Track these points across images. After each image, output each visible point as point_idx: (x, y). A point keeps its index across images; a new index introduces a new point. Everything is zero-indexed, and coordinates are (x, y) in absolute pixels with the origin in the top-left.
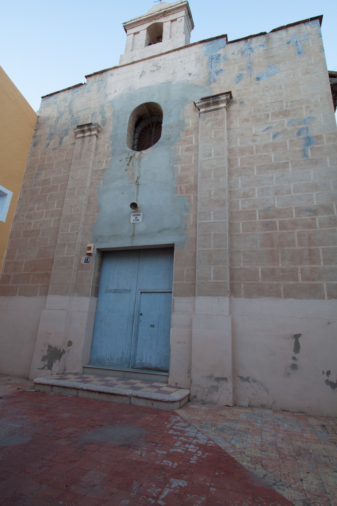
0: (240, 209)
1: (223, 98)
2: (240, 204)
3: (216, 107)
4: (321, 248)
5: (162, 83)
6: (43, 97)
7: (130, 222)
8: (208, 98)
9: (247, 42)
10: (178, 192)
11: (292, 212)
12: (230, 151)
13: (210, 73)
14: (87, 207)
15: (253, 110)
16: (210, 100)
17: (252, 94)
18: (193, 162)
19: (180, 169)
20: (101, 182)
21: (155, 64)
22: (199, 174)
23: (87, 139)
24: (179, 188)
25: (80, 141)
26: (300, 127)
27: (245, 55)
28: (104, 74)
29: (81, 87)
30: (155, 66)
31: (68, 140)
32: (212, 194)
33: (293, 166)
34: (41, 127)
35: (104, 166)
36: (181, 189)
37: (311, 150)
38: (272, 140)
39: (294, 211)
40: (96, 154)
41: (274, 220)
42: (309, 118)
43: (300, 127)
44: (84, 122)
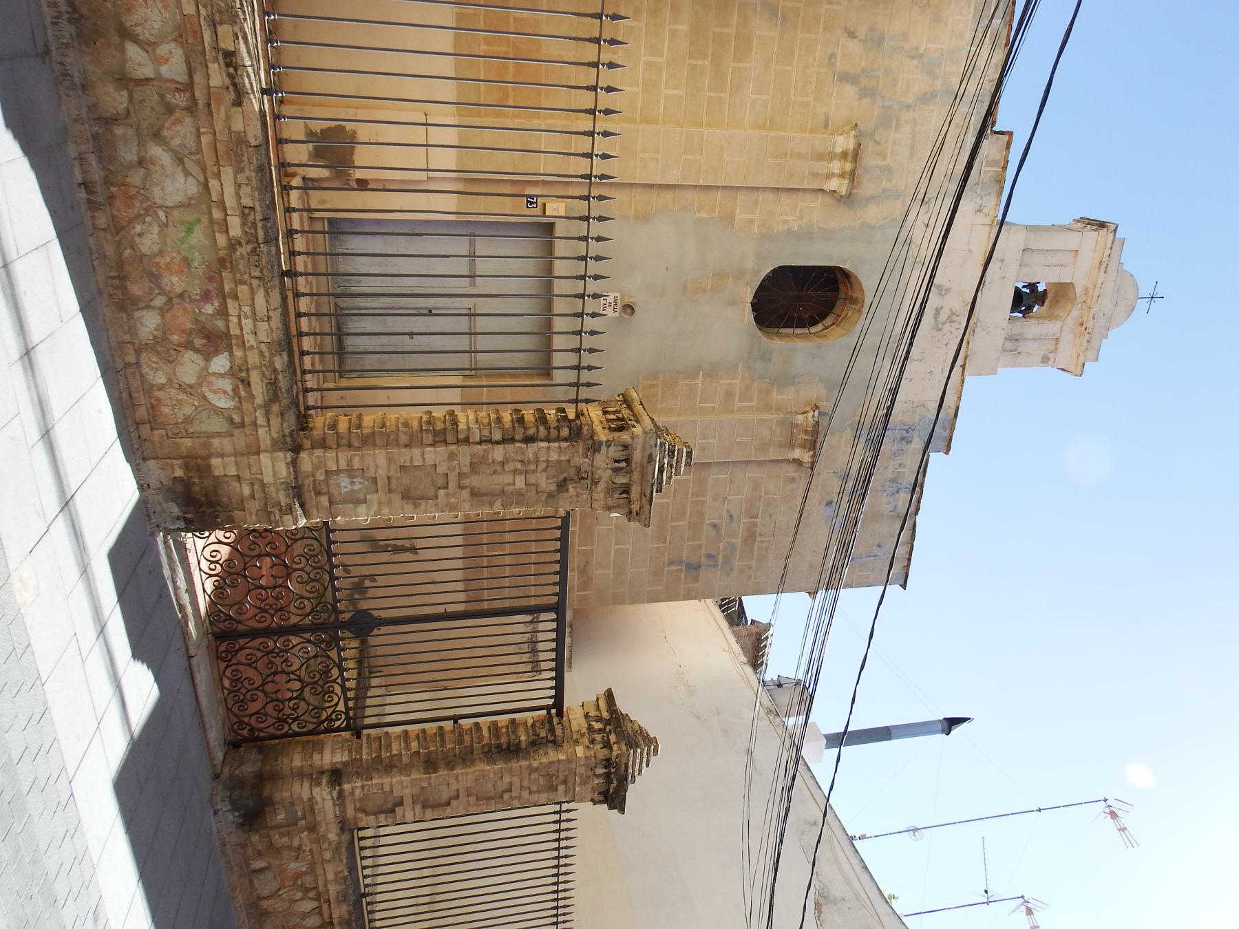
3: (476, 528)
4: (726, 95)
20: (705, 215)
33: (657, 548)
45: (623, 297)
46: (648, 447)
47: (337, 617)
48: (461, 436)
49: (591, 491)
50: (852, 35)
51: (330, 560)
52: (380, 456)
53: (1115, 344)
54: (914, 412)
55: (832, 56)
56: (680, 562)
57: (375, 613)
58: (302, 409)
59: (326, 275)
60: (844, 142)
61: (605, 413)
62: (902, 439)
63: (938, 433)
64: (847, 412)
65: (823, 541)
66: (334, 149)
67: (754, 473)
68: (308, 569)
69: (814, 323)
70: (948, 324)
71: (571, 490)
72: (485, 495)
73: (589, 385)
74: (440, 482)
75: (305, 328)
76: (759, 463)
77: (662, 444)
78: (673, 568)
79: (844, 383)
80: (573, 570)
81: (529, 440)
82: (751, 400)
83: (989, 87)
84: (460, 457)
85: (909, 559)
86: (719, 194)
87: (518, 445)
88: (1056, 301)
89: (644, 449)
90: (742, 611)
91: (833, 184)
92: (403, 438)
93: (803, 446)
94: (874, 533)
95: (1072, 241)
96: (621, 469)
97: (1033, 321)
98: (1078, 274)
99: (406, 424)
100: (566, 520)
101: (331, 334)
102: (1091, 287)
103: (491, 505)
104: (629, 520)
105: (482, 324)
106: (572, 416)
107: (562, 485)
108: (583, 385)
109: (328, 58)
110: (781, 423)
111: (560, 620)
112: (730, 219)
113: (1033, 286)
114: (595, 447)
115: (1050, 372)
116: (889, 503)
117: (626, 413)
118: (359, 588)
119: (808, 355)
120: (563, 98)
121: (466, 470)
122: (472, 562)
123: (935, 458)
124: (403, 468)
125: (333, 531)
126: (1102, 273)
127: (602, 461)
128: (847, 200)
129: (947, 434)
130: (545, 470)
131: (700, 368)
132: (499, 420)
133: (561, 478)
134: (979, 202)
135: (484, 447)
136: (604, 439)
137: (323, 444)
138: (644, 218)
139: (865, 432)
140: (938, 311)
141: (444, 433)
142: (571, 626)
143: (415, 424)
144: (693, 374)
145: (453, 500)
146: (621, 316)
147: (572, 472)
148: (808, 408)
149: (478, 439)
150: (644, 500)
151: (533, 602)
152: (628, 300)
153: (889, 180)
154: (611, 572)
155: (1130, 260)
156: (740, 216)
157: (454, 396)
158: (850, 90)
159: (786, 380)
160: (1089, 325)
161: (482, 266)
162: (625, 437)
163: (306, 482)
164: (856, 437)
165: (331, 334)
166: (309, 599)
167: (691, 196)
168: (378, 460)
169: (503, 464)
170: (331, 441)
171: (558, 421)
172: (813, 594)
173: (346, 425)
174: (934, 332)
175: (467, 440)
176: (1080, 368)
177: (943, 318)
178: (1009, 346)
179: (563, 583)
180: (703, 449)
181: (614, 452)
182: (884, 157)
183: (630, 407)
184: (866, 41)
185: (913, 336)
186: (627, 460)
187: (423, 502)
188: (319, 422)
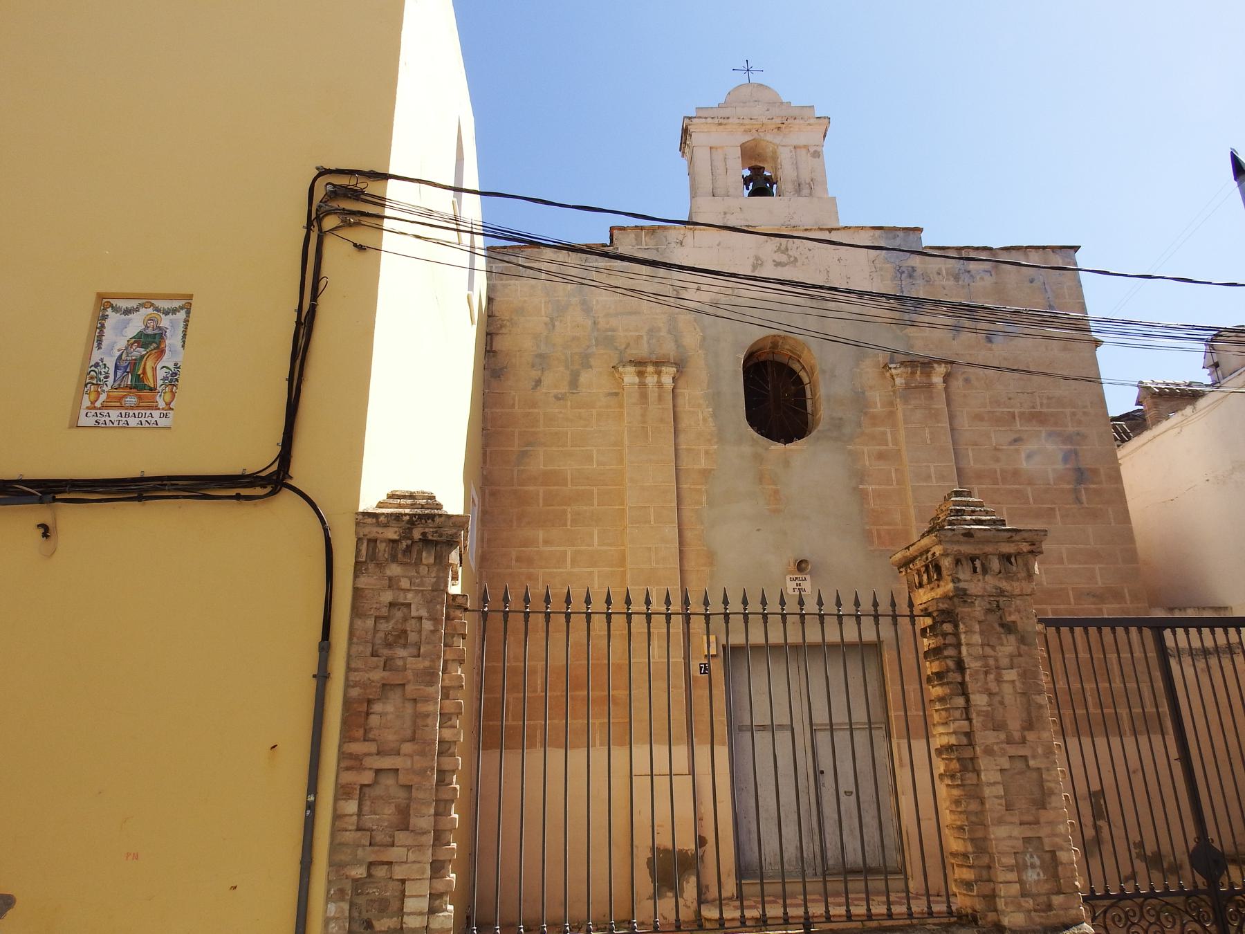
3: (1068, 722)
4: (595, 489)
20: (704, 498)
39: (1071, 593)
45: (790, 573)
46: (955, 538)
47: (1203, 892)
48: (964, 741)
49: (1012, 596)
50: (538, 382)
51: (1129, 897)
52: (998, 832)
53: (793, 94)
54: (881, 269)
55: (557, 398)
56: (1076, 491)
57: (1192, 844)
58: (953, 920)
59: (784, 883)
60: (630, 376)
61: (921, 585)
62: (910, 276)
63: (900, 243)
64: (888, 338)
65: (1029, 342)
66: (670, 869)
67: (963, 422)
68: (1144, 924)
69: (799, 381)
70: (790, 253)
71: (1013, 618)
72: (1029, 713)
73: (893, 604)
74: (1020, 765)
75: (883, 910)
76: (952, 417)
77: (950, 523)
78: (1084, 498)
79: (857, 344)
80: (1100, 610)
81: (960, 666)
82: (884, 433)
83: (574, 258)
84: (989, 742)
85: (1044, 248)
86: (684, 486)
87: (967, 678)
88: (760, 157)
89: (958, 542)
90: (1126, 417)
91: (667, 380)
92: (974, 806)
93: (929, 375)
94: (1020, 292)
95: (702, 156)
96: (983, 565)
97: (779, 173)
98: (731, 142)
99: (957, 802)
100: (1057, 623)
101: (866, 881)
102: (743, 128)
103: (1041, 707)
104: (1041, 553)
105: (820, 717)
106: (929, 621)
107: (1009, 628)
108: (894, 611)
109: (577, 871)
110: (906, 400)
111: (1174, 624)
112: (706, 474)
113: (746, 181)
114: (961, 595)
115: (828, 148)
116: (982, 279)
117: (919, 564)
118: (1155, 861)
119: (833, 380)
120: (618, 644)
121: (1003, 736)
122: (1110, 726)
123: (928, 240)
124: (1009, 807)
125: (1092, 891)
126: (730, 121)
127: (975, 586)
128: (680, 365)
129: (901, 234)
130: (993, 647)
131: (855, 489)
132: (941, 699)
133: (1001, 630)
134: (673, 245)
135: (974, 716)
136: (951, 586)
137: (991, 898)
138: (711, 557)
139: (906, 316)
140: (778, 264)
141: (963, 760)
142: (1171, 609)
143: (956, 792)
144: (863, 495)
145: (1040, 751)
146: (810, 573)
147: (991, 617)
148: (888, 374)
149: (966, 723)
150: (1017, 538)
151: (1152, 655)
152: (793, 567)
153: (659, 330)
154: (1097, 567)
155: (713, 97)
156: (703, 463)
157: (919, 746)
158: (584, 378)
159: (859, 400)
160: (779, 121)
161: (782, 718)
162: (946, 563)
163: (1037, 920)
164: (913, 324)
165: (866, 881)
166: (1183, 926)
167: (688, 513)
168: (1004, 836)
169: (991, 694)
170: (987, 889)
171: (936, 636)
172: (1098, 343)
173: (965, 870)
174: (798, 264)
175: (969, 735)
176: (821, 121)
177: (784, 258)
178: (806, 191)
179: (1126, 623)
180: (942, 478)
181: (964, 574)
182: (640, 337)
183: (912, 560)
184: (543, 370)
185: (814, 286)
186: (973, 559)
187: (1047, 785)
188: (962, 902)
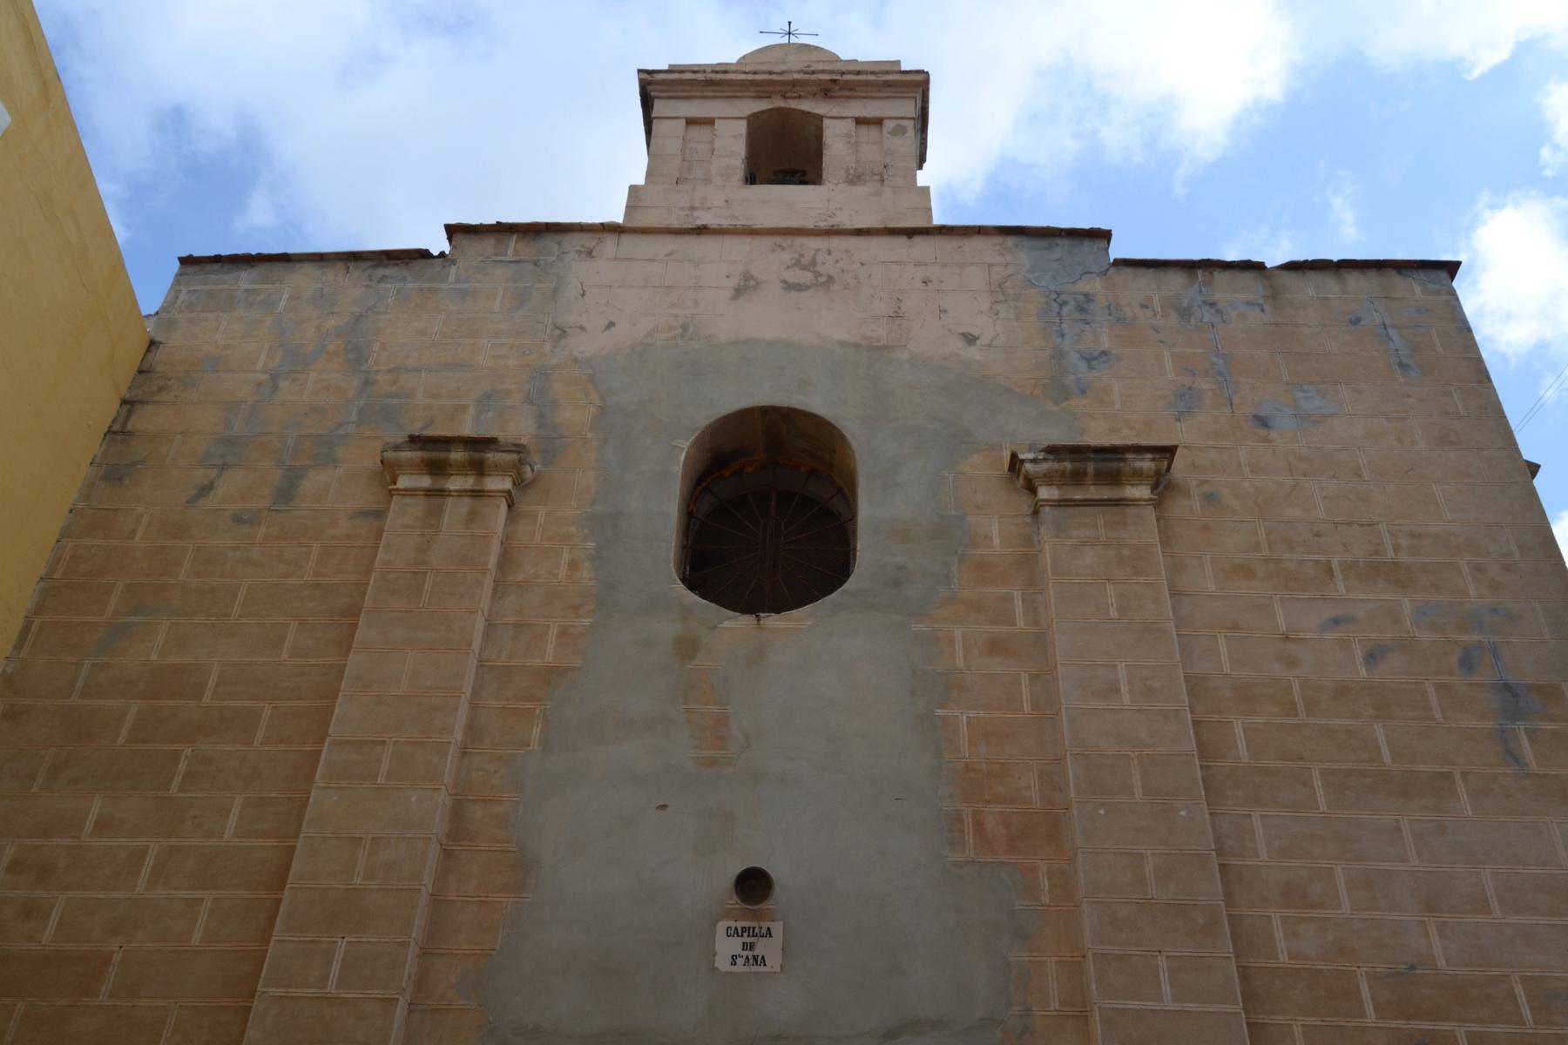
0: (1284, 958)
1: (1146, 464)
2: (1279, 934)
3: (1107, 493)
5: (842, 344)
6: (186, 261)
7: (714, 969)
8: (1077, 452)
9: (832, 221)
10: (970, 838)
11: (1512, 997)
12: (1196, 686)
13: (1059, 354)
14: (447, 854)
15: (1262, 536)
16: (1087, 459)
17: (1247, 470)
18: (1026, 707)
19: (964, 731)
20: (536, 732)
21: (804, 261)
22: (1072, 769)
23: (455, 510)
24: (969, 823)
25: (416, 507)
26: (1465, 638)
27: (1193, 320)
28: (549, 242)
29: (418, 264)
30: (804, 268)
31: (336, 490)
32: (1149, 870)
34: (164, 396)
35: (550, 653)
36: (979, 827)
37: (1529, 737)
38: (1363, 673)
40: (500, 588)
41: (1445, 1026)
42: (1495, 610)
43: (1465, 638)
44: (431, 422)
